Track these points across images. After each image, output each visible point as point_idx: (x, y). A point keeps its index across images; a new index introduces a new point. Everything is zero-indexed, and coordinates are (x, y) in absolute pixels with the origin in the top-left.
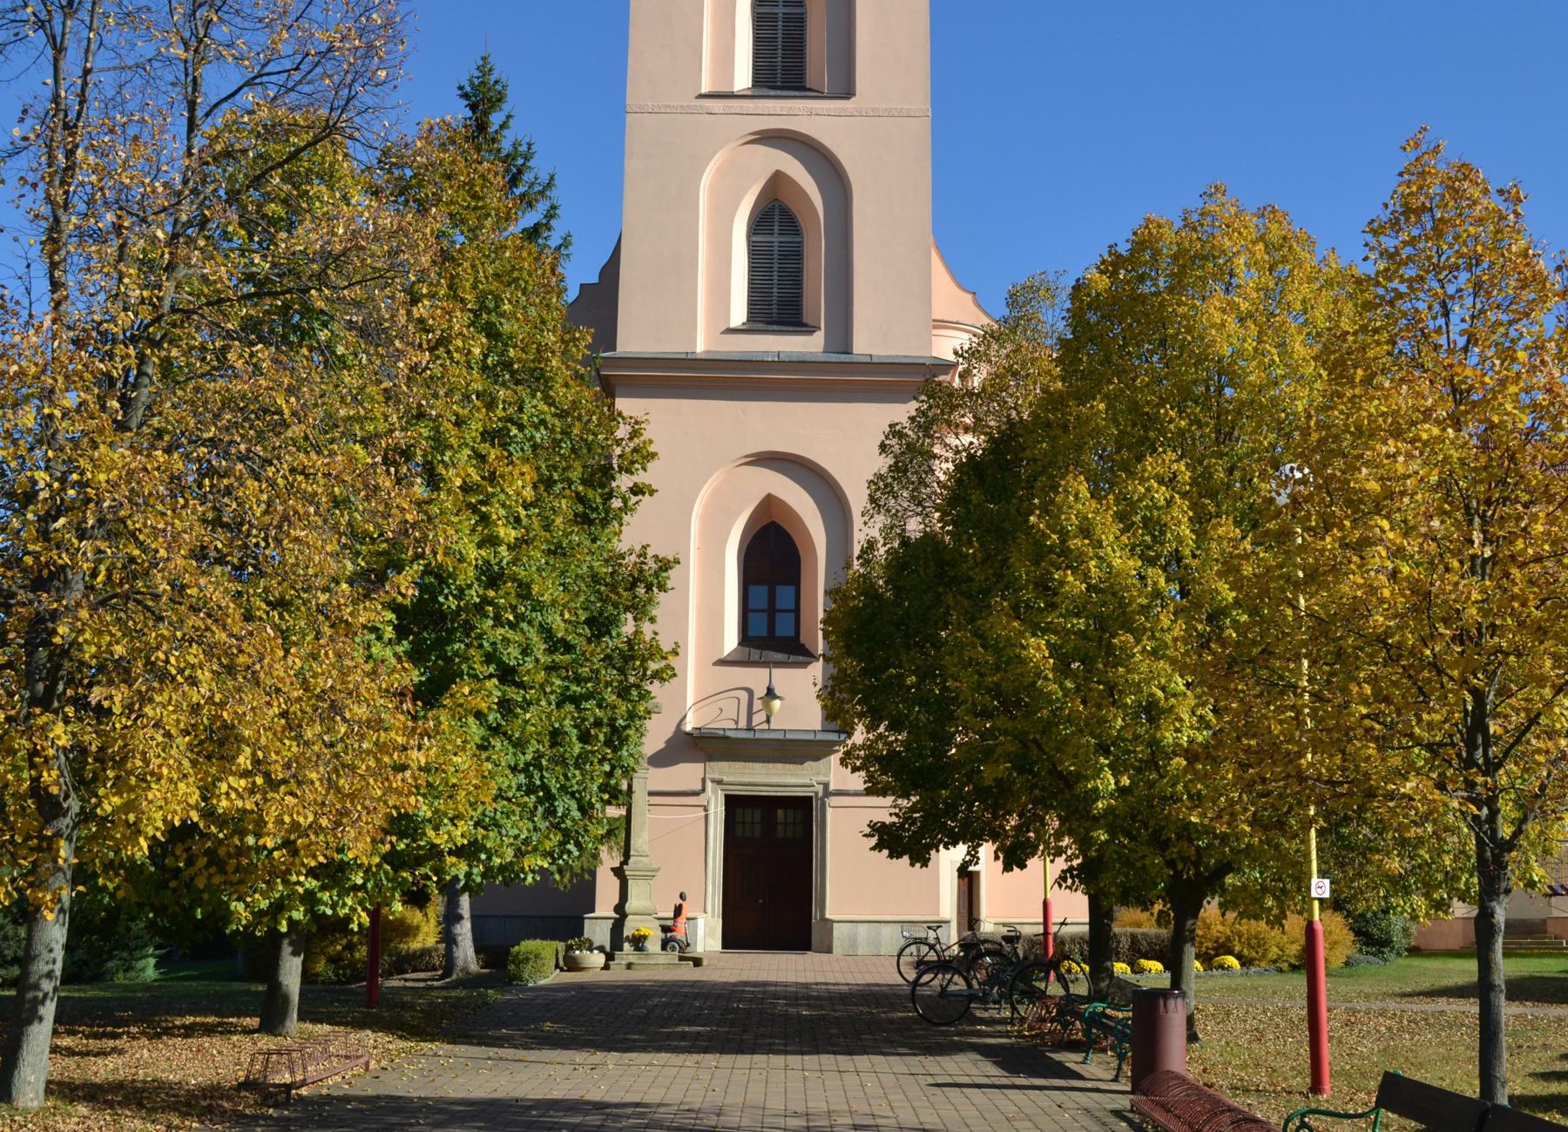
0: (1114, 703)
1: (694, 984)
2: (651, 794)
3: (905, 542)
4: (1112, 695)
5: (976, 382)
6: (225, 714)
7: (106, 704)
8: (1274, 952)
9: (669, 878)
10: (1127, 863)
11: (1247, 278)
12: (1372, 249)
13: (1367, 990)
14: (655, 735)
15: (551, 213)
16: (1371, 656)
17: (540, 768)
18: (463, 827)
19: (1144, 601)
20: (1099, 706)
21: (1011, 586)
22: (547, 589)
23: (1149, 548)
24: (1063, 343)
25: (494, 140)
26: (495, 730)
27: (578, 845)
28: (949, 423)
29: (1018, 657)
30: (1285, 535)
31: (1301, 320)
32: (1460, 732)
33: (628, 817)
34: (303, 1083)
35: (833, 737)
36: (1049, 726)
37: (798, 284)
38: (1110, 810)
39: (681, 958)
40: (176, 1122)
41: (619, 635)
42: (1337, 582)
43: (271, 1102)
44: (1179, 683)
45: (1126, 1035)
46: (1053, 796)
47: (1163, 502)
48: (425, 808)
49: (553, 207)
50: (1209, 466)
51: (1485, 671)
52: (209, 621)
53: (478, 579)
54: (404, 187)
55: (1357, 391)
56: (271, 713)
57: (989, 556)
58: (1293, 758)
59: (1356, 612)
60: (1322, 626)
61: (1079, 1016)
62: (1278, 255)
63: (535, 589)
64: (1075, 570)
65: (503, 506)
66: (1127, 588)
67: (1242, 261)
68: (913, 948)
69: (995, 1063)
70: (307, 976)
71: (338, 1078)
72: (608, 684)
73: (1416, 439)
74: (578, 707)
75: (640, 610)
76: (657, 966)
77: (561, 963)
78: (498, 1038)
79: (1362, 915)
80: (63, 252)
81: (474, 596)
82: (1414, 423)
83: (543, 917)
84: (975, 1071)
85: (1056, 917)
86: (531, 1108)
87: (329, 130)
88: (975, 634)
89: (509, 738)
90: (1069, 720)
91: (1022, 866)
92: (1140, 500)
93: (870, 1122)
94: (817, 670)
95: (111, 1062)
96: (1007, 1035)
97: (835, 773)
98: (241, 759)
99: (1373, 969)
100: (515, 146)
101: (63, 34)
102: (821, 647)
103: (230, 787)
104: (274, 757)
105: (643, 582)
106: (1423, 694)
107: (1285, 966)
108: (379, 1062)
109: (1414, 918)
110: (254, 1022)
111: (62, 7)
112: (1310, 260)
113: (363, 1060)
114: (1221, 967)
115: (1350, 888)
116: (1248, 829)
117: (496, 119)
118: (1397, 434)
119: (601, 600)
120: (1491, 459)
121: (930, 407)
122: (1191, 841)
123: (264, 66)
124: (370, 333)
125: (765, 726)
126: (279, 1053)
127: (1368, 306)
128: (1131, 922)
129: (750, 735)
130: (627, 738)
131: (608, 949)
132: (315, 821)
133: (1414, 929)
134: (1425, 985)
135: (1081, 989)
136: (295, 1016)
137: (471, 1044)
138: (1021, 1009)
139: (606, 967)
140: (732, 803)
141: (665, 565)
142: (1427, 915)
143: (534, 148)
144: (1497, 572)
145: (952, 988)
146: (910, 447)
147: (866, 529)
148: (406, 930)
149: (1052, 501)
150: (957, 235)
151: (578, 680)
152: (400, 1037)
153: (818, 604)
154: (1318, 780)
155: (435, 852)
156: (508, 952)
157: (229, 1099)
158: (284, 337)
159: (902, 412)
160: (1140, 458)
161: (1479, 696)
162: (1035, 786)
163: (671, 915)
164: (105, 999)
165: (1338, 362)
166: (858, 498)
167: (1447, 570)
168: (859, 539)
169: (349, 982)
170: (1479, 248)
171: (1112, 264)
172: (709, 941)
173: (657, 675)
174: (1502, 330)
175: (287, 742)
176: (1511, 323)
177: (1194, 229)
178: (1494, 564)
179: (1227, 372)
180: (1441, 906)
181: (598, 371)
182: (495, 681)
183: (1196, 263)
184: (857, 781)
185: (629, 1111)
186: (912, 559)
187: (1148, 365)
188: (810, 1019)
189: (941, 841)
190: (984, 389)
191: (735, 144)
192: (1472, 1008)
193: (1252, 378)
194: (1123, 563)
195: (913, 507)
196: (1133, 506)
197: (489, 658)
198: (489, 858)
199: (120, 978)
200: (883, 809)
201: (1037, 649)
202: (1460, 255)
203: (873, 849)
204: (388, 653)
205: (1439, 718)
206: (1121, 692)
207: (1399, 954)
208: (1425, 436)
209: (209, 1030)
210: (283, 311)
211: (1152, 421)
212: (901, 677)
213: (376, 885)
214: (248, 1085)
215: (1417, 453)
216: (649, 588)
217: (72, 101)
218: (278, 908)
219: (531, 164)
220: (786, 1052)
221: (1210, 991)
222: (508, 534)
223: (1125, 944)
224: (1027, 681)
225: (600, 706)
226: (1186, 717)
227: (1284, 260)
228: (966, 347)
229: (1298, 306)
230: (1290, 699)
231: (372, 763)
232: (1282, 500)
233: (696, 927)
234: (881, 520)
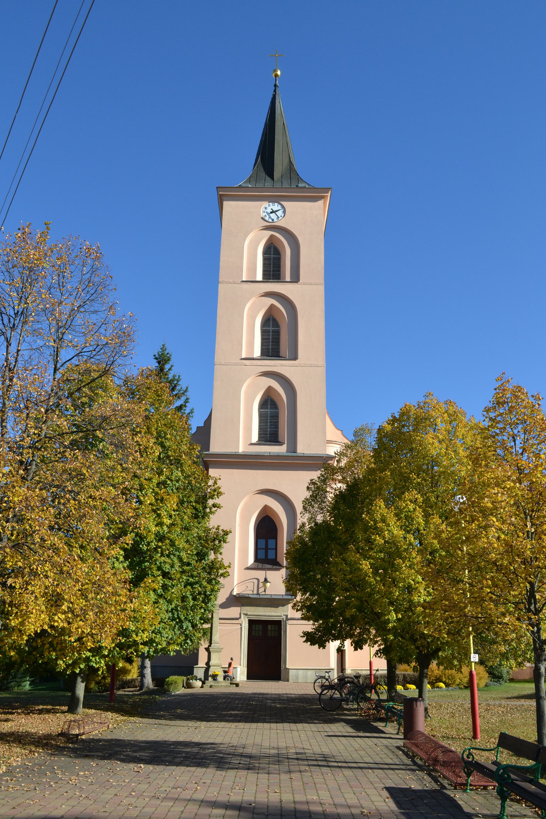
0: (395, 586)
1: (236, 694)
2: (220, 619)
3: (316, 524)
4: (394, 583)
5: (342, 464)
6: (58, 590)
7: (13, 585)
8: (458, 681)
9: (227, 651)
10: (401, 648)
11: (441, 426)
12: (486, 417)
13: (494, 696)
14: (222, 596)
15: (187, 401)
16: (491, 569)
17: (177, 611)
18: (146, 634)
19: (406, 547)
20: (389, 587)
21: (355, 541)
22: (181, 543)
23: (408, 527)
24: (375, 450)
25: (166, 374)
26: (160, 596)
27: (191, 640)
28: (333, 479)
29: (359, 568)
30: (458, 523)
31: (462, 442)
32: (525, 598)
33: (211, 628)
34: (83, 734)
35: (289, 597)
36: (370, 595)
37: (277, 427)
38: (394, 627)
39: (231, 684)
40: (33, 749)
41: (208, 559)
42: (477, 541)
43: (70, 741)
44: (420, 578)
45: (401, 716)
46: (373, 621)
47: (412, 510)
48: (132, 626)
49: (187, 399)
50: (429, 496)
51: (534, 575)
52: (54, 554)
53: (155, 539)
54: (132, 392)
55: (483, 470)
56: (75, 589)
57: (348, 530)
58: (462, 609)
59: (484, 552)
60: (472, 557)
61: (383, 708)
62: (452, 418)
63: (177, 543)
64: (379, 535)
65: (166, 510)
66: (399, 542)
67: (439, 420)
68: (320, 680)
69: (351, 727)
70: (87, 690)
71: (97, 732)
72: (204, 578)
73: (505, 487)
74: (193, 588)
75: (216, 550)
76: (221, 687)
77: (185, 685)
78: (159, 716)
79: (491, 666)
80: (6, 416)
81: (153, 545)
82: (504, 481)
83: (178, 667)
84: (343, 730)
85: (374, 667)
86: (171, 745)
87: (105, 372)
88: (342, 559)
89: (166, 599)
90: (378, 592)
91: (361, 648)
92: (404, 509)
93: (302, 751)
94: (283, 572)
95: (9, 724)
96: (356, 715)
97: (289, 611)
98: (63, 607)
99: (496, 688)
100: (174, 376)
101: (11, 337)
102: (285, 563)
103: (59, 618)
104: (76, 606)
105: (219, 539)
106: (511, 583)
107: (462, 687)
108: (113, 725)
109: (511, 668)
110: (65, 708)
111: (11, 328)
112: (465, 420)
113: (107, 724)
114: (438, 687)
115: (486, 656)
116: (446, 636)
117: (167, 367)
118: (497, 485)
119: (201, 546)
120: (533, 495)
121: (325, 474)
122: (425, 639)
123: (83, 349)
124: (120, 446)
125: (264, 593)
126: (74, 721)
127: (485, 438)
128: (404, 670)
129: (258, 596)
130: (210, 599)
131: (203, 679)
132: (91, 631)
133: (511, 672)
134: (516, 694)
135: (384, 697)
136: (81, 706)
137: (149, 718)
138: (361, 704)
139: (202, 687)
140: (252, 623)
141: (226, 533)
142: (516, 667)
143: (181, 377)
144: (537, 538)
145: (335, 696)
146: (318, 488)
147: (302, 519)
148: (125, 671)
149: (371, 509)
150: (335, 410)
151: (192, 576)
152: (122, 715)
153: (284, 547)
154: (472, 617)
155: (135, 643)
156: (165, 681)
157: (54, 740)
158: (86, 447)
159: (315, 475)
160: (403, 493)
161: (532, 584)
162: (365, 617)
163: (227, 666)
164: (9, 698)
165: (476, 459)
166: (299, 508)
167: (518, 537)
168: (299, 522)
169: (103, 692)
170: (525, 417)
171: (392, 420)
172: (242, 676)
173: (222, 575)
174: (535, 447)
175: (81, 600)
176: (538, 444)
177: (422, 408)
178: (536, 534)
179: (435, 462)
180: (520, 664)
181: (203, 459)
182: (161, 577)
183: (422, 421)
184: (299, 615)
185: (209, 746)
186: (318, 530)
187: (405, 457)
188: (280, 708)
189: (330, 638)
190: (346, 467)
191: (254, 376)
192: (533, 703)
193: (444, 463)
194: (398, 532)
195: (319, 510)
196: (401, 511)
197: (159, 568)
198: (157, 645)
199: (16, 689)
200: (309, 626)
201: (366, 565)
202: (518, 419)
203: (304, 642)
204: (121, 566)
205: (517, 592)
206: (398, 582)
207: (506, 682)
208: (508, 486)
209: (48, 711)
210: (86, 438)
211: (407, 479)
212: (315, 575)
213: (112, 656)
214: (62, 734)
215: (505, 493)
216: (220, 542)
217: (12, 360)
218: (75, 663)
219: (179, 383)
220: (270, 722)
221: (434, 697)
222: (167, 521)
223: (401, 678)
224: (362, 577)
225: (200, 587)
226: (422, 591)
227: (455, 420)
228: (339, 451)
229: (461, 437)
230: (461, 585)
231: (113, 609)
232: (456, 510)
233: (237, 671)
234: (307, 515)
